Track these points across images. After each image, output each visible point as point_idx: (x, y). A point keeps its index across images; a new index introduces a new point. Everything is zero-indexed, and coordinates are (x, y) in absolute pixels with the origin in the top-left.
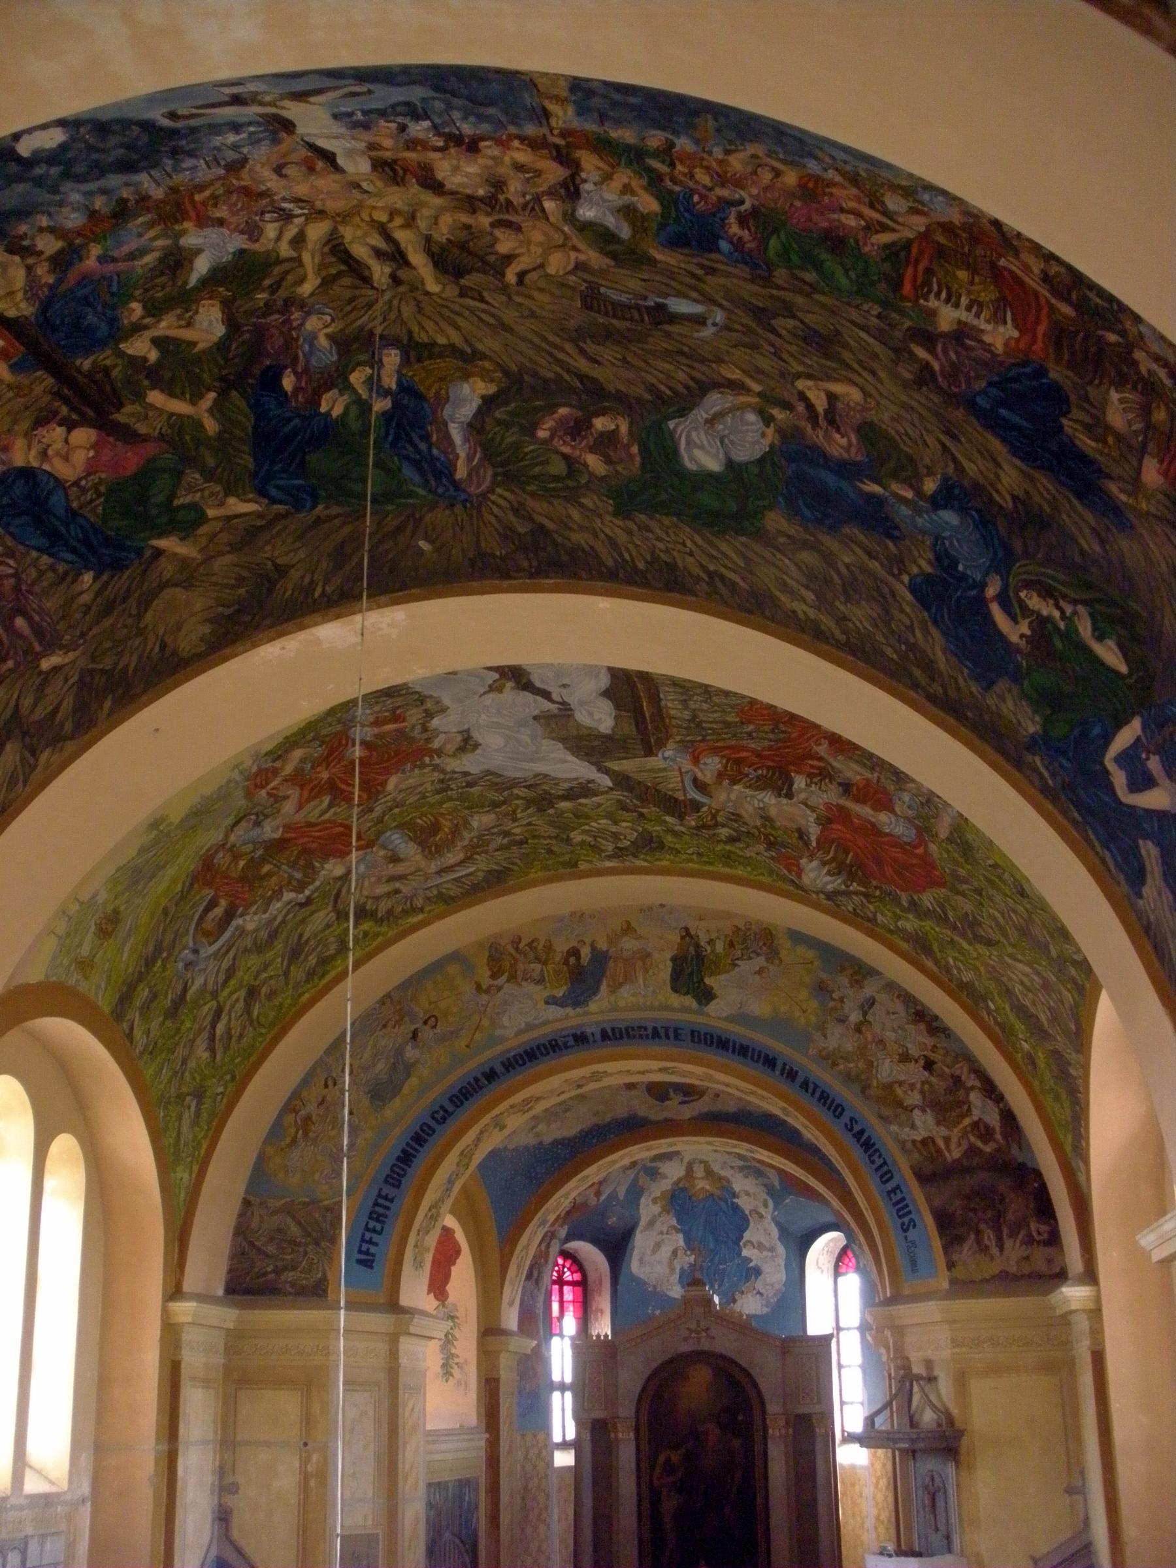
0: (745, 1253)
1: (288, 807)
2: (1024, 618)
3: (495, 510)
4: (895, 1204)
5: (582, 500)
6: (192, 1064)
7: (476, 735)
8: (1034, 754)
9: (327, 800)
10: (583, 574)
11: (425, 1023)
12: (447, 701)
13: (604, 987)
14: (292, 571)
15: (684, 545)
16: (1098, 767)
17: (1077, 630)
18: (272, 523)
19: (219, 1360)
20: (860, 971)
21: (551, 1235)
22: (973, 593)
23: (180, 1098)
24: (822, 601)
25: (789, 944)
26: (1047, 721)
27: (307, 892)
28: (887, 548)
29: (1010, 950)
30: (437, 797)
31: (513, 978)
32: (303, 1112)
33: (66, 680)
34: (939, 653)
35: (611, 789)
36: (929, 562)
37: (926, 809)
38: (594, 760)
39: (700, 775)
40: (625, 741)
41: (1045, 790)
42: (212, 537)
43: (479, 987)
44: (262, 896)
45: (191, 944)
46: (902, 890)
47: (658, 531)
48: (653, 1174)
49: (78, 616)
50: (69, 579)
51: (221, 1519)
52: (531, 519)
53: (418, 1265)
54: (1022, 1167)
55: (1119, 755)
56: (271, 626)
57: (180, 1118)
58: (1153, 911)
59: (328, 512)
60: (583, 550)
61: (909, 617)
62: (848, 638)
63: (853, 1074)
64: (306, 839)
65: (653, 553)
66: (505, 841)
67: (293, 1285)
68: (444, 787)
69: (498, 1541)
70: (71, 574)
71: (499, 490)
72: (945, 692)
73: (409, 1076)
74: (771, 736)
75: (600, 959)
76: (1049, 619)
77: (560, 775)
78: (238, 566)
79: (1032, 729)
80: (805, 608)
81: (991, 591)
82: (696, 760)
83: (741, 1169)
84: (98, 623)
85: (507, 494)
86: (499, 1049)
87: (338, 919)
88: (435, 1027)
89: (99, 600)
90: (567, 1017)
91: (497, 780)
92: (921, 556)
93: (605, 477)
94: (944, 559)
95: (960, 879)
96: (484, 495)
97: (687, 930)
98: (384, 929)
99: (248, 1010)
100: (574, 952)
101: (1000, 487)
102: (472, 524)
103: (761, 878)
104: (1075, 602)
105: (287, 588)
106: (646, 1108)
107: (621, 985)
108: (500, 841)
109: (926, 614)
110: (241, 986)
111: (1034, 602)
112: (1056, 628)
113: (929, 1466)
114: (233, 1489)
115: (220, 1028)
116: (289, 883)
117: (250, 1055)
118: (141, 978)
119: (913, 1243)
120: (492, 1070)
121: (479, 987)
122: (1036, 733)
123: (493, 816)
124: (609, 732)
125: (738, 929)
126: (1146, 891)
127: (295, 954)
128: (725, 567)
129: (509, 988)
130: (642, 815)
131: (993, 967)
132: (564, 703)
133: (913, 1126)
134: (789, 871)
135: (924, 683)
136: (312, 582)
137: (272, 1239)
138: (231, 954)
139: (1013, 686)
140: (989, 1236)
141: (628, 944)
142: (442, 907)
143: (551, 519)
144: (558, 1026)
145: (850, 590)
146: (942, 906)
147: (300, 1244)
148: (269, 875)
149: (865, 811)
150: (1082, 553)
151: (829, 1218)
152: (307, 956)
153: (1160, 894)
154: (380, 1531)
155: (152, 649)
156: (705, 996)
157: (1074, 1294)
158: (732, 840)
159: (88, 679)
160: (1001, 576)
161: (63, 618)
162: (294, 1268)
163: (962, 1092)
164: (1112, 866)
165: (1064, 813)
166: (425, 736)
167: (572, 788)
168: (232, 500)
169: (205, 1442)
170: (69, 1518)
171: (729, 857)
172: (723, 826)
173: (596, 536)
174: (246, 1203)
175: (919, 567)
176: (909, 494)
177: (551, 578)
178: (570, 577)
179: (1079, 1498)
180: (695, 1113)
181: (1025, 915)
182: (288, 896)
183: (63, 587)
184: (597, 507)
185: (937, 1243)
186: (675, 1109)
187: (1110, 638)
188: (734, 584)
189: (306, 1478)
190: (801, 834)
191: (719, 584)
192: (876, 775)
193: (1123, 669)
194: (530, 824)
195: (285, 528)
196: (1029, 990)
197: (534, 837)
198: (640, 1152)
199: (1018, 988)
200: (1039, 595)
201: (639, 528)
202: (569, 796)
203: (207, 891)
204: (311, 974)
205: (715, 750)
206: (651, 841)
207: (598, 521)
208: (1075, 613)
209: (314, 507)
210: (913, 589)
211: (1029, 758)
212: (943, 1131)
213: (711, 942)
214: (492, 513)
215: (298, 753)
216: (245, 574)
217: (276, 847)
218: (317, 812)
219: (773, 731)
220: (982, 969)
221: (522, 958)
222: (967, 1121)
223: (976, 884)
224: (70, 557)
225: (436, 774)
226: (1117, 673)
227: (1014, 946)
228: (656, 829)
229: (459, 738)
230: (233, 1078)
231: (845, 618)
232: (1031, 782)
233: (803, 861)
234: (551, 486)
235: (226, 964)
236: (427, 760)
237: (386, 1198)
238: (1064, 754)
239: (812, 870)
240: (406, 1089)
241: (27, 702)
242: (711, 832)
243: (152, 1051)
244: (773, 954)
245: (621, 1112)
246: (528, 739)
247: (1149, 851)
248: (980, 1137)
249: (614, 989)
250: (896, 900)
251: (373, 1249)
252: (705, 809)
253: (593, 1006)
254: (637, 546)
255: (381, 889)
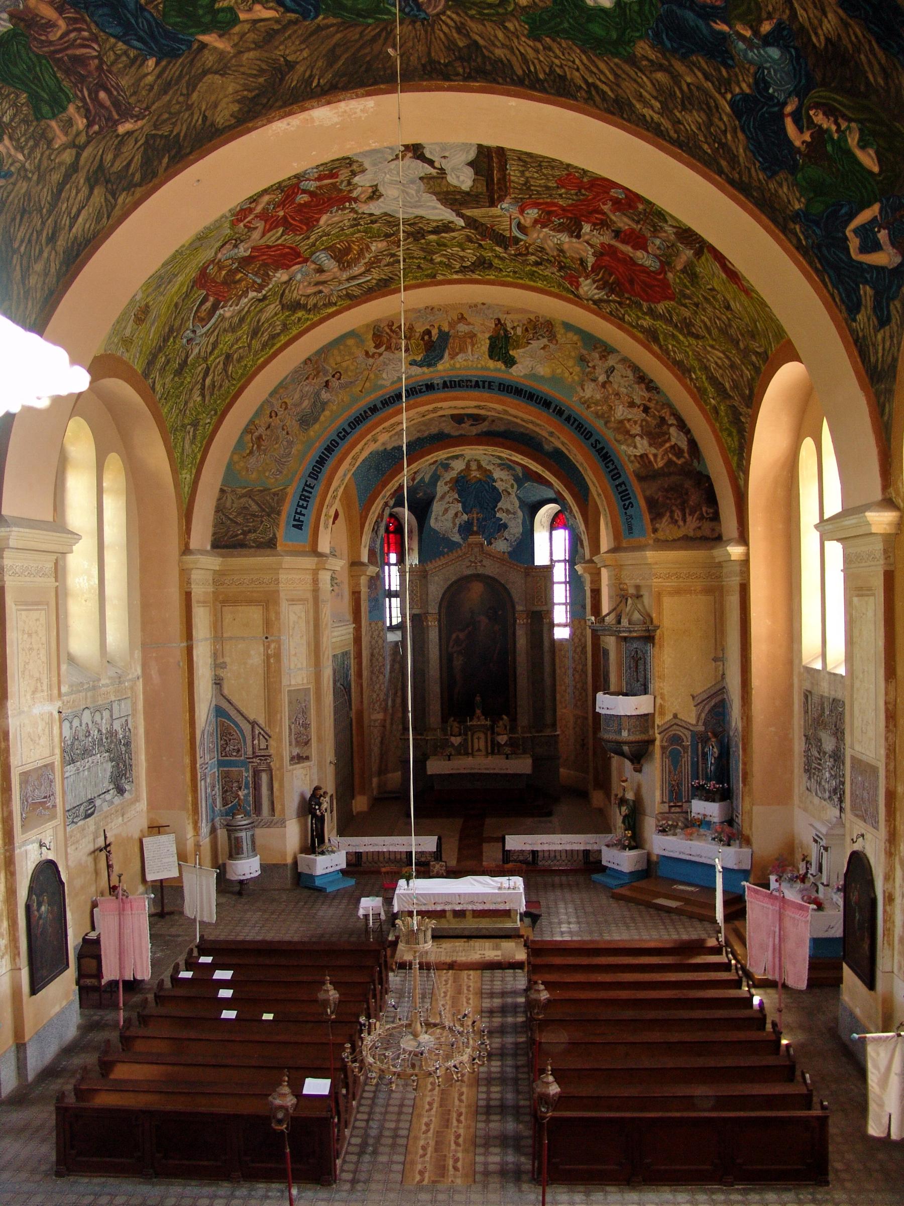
0: (498, 515)
1: (256, 235)
2: (808, 129)
3: (444, 28)
4: (620, 493)
5: (507, 24)
6: (191, 405)
7: (381, 189)
8: (795, 223)
9: (281, 230)
10: (501, 80)
11: (333, 376)
12: (367, 165)
13: (446, 355)
14: (298, 66)
15: (573, 62)
16: (840, 235)
17: (847, 140)
18: (285, 28)
19: (211, 589)
20: (606, 350)
21: (386, 504)
22: (776, 109)
23: (184, 426)
24: (666, 110)
25: (562, 331)
26: (809, 201)
27: (264, 292)
28: (720, 72)
29: (711, 342)
30: (351, 230)
31: (388, 348)
32: (256, 434)
33: (136, 142)
34: (741, 151)
35: (463, 227)
36: (749, 86)
37: (670, 250)
38: (455, 208)
39: (522, 221)
40: (477, 196)
41: (799, 247)
42: (242, 35)
43: (367, 353)
44: (235, 295)
45: (191, 327)
46: (644, 300)
47: (557, 51)
48: (446, 467)
49: (144, 93)
50: (138, 62)
51: (216, 684)
52: (467, 36)
53: (326, 527)
54: (700, 473)
55: (857, 228)
56: (281, 107)
57: (184, 439)
58: (862, 330)
59: (326, 21)
60: (502, 62)
61: (725, 125)
62: (679, 137)
63: (600, 413)
64: (265, 257)
65: (551, 67)
66: (391, 260)
67: (254, 541)
68: (356, 223)
69: (361, 685)
70: (140, 59)
71: (449, 13)
72: (741, 178)
73: (323, 410)
74: (575, 197)
75: (444, 337)
76: (828, 131)
77: (431, 217)
78: (260, 60)
79: (797, 207)
80: (651, 113)
81: (789, 109)
82: (522, 211)
83: (499, 465)
84: (159, 99)
85: (454, 16)
86: (381, 392)
87: (282, 309)
88: (339, 379)
89: (159, 81)
90: (424, 373)
91: (391, 220)
92: (744, 80)
93: (526, 7)
94: (761, 83)
95: (685, 296)
96: (438, 15)
97: (499, 320)
98: (311, 316)
99: (225, 370)
100: (428, 332)
101: (820, 32)
102: (426, 38)
103: (552, 289)
104: (850, 120)
105: (293, 80)
106: (449, 428)
107: (457, 354)
108: (388, 260)
109: (737, 123)
110: (222, 354)
111: (819, 119)
112: (832, 138)
113: (635, 646)
114: (223, 666)
115: (208, 381)
116: (253, 286)
117: (226, 398)
118: (160, 349)
119: (631, 517)
120: (375, 406)
121: (367, 353)
122: (800, 209)
123: (385, 244)
124: (468, 190)
125: (531, 320)
126: (859, 317)
127: (255, 333)
128: (600, 80)
129: (386, 354)
130: (480, 245)
131: (698, 352)
132: (442, 169)
133: (635, 447)
134: (571, 285)
135: (726, 170)
136: (311, 76)
137: (239, 514)
138: (216, 333)
139: (789, 176)
140: (678, 514)
141: (462, 328)
142: (349, 302)
143: (482, 38)
144: (418, 378)
145: (687, 102)
146: (669, 311)
147: (257, 516)
148: (240, 280)
149: (627, 249)
150: (868, 83)
151: (551, 495)
152: (262, 334)
153: (869, 320)
154: (311, 686)
155: (197, 121)
156: (510, 362)
157: (735, 551)
158: (537, 264)
159: (151, 142)
160: (799, 100)
161: (134, 93)
162: (255, 531)
163: (665, 427)
164: (837, 300)
165: (811, 263)
166: (348, 188)
167: (438, 226)
168: (258, 7)
169: (206, 639)
170: (132, 688)
171: (533, 275)
172: (532, 254)
173: (513, 53)
174: (222, 491)
175: (741, 88)
176: (748, 34)
177: (478, 82)
178: (491, 82)
179: (720, 663)
180: (479, 431)
181: (726, 322)
182: (252, 294)
183: (133, 69)
184: (516, 29)
185: (647, 517)
186: (467, 428)
187: (872, 148)
188: (604, 93)
189: (268, 657)
190: (582, 262)
191: (594, 93)
192: (639, 226)
193: (876, 169)
194: (408, 249)
195: (295, 31)
196: (720, 367)
197: (410, 258)
198: (442, 455)
199: (713, 366)
200: (825, 114)
201: (544, 48)
202: (436, 231)
203: (202, 291)
204: (265, 346)
205: (536, 205)
206: (484, 263)
207: (516, 41)
208: (848, 128)
209: (316, 17)
210: (732, 104)
211: (792, 226)
212: (654, 451)
213: (514, 328)
214: (442, 30)
215: (266, 198)
216: (264, 66)
217: (246, 262)
218: (273, 238)
219: (576, 194)
220: (690, 353)
221: (394, 335)
222: (668, 445)
223: (696, 300)
224: (139, 45)
225: (352, 214)
226: (870, 172)
227: (715, 340)
228: (488, 255)
229: (370, 190)
230: (216, 413)
231: (679, 122)
232: (791, 242)
233: (581, 279)
234: (486, 11)
235: (212, 340)
236: (347, 204)
237: (309, 486)
238: (818, 225)
239: (586, 285)
240: (322, 418)
241: (109, 157)
242: (524, 258)
243: (166, 397)
244: (552, 337)
245: (434, 430)
246: (413, 192)
247: (867, 292)
248: (675, 455)
249: (452, 357)
250: (640, 307)
251: (302, 518)
252: (522, 243)
253: (440, 367)
254: (540, 61)
255: (310, 291)
